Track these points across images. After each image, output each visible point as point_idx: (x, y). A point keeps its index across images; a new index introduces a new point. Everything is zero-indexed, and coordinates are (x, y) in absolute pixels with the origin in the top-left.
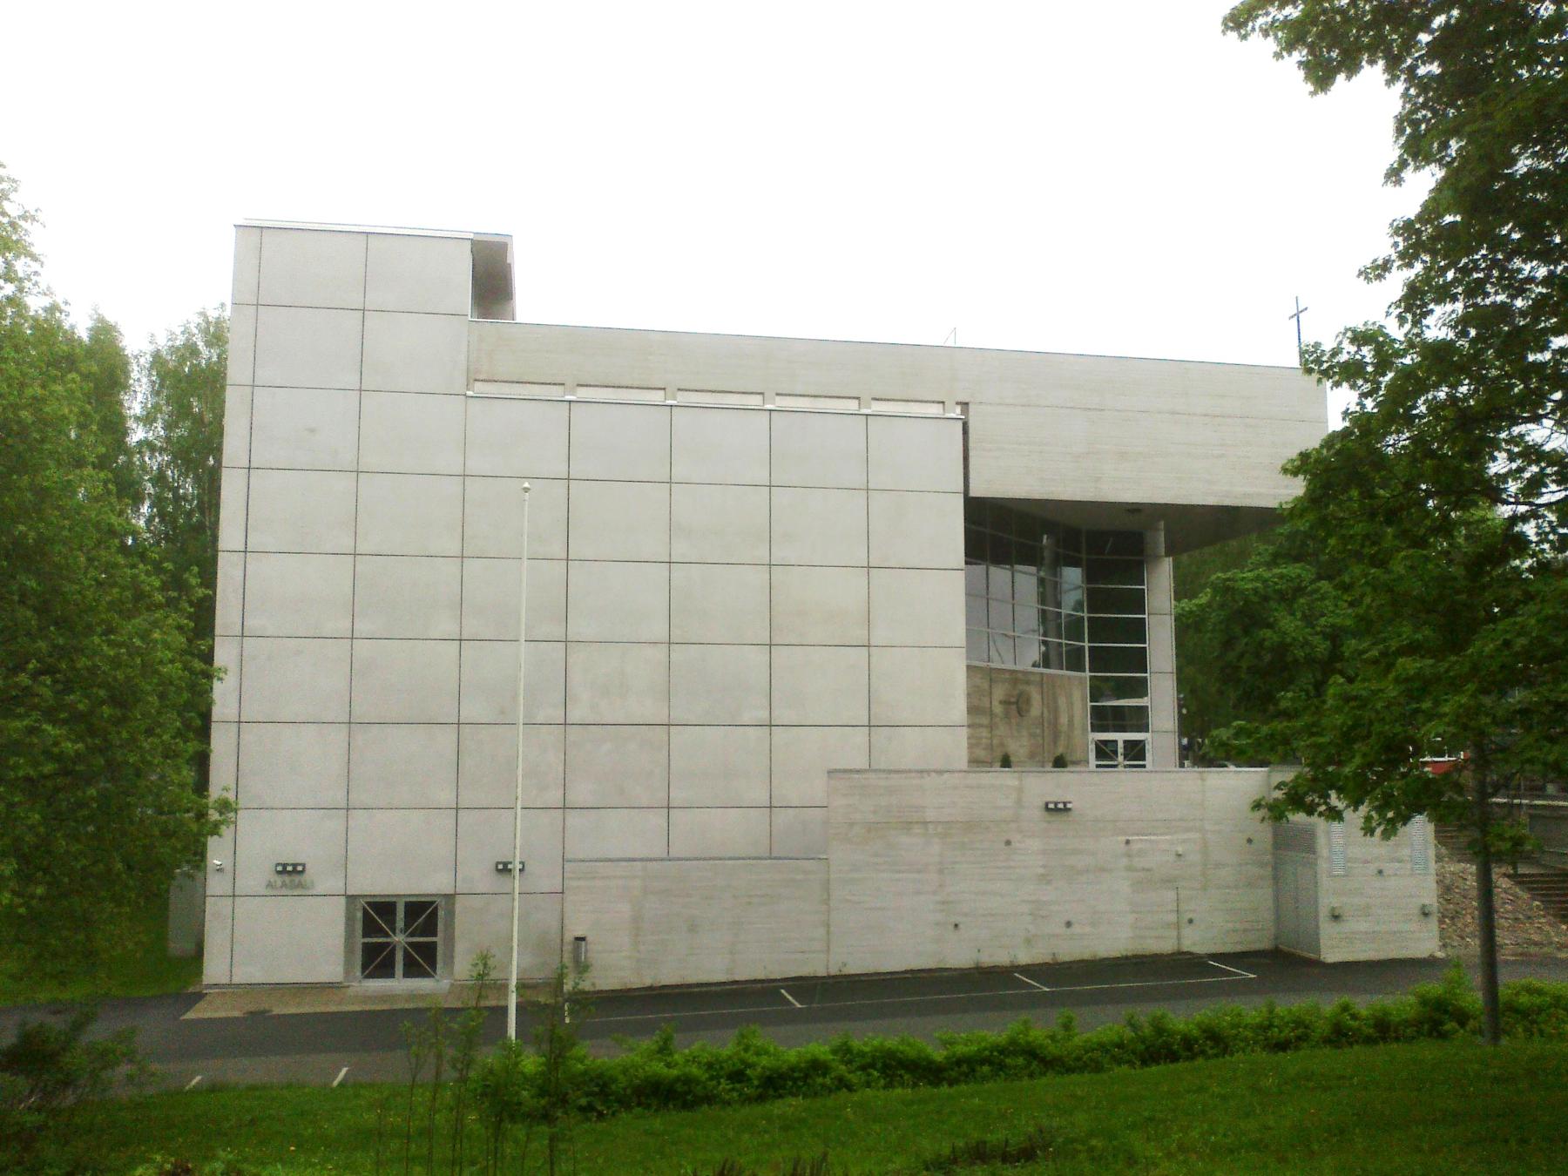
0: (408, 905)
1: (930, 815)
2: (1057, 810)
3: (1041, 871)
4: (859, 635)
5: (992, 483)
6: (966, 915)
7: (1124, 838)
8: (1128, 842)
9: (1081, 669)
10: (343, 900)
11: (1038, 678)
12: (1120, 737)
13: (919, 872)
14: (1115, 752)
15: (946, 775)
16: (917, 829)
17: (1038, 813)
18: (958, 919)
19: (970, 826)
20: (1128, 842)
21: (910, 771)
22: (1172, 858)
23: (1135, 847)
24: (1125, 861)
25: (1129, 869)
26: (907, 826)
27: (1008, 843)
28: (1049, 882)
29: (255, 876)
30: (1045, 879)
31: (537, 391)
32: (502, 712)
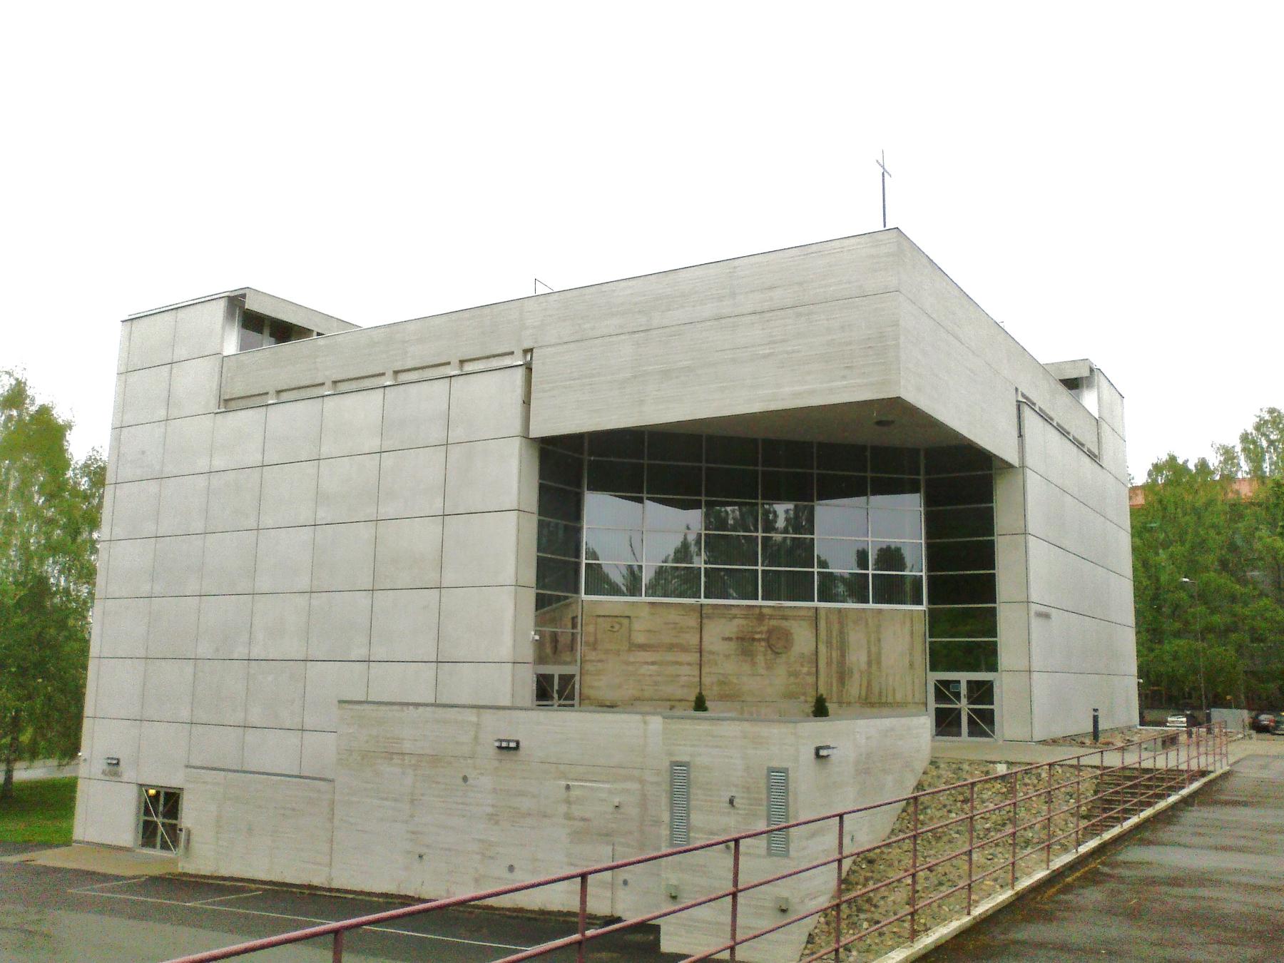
0: (166, 794)
1: (407, 746)
2: (509, 748)
3: (490, 810)
4: (431, 577)
5: (550, 424)
6: (428, 846)
7: (564, 783)
8: (568, 787)
9: (920, 603)
10: (135, 789)
11: (811, 613)
12: (964, 677)
13: (396, 800)
14: (957, 696)
15: (421, 709)
16: (396, 760)
17: (491, 751)
18: (423, 850)
19: (436, 760)
20: (568, 787)
21: (464, 706)
22: (611, 809)
23: (574, 793)
24: (563, 808)
25: (568, 817)
26: (390, 755)
27: (465, 779)
28: (497, 823)
29: (98, 766)
30: (493, 818)
31: (304, 393)
32: (217, 650)
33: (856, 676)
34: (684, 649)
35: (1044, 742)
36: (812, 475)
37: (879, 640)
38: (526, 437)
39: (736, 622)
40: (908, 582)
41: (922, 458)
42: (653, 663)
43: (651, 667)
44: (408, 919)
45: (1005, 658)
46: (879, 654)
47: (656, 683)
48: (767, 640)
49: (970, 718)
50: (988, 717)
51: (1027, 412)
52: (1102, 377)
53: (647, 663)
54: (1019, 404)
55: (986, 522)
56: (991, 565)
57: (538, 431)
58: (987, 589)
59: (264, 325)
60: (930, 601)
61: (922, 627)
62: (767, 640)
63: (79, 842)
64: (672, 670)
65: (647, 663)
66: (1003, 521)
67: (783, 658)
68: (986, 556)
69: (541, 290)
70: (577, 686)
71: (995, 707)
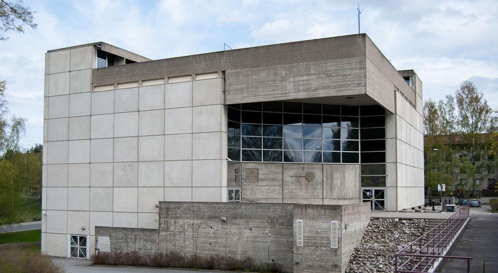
12: (373, 189)
33: (336, 189)
34: (276, 180)
35: (399, 211)
36: (323, 114)
37: (344, 176)
38: (224, 105)
39: (295, 170)
40: (245, 134)
41: (280, 150)
42: (266, 186)
43: (266, 187)
44: (377, 50)
45: (389, 181)
46: (344, 181)
47: (268, 193)
48: (306, 177)
49: (375, 204)
50: (382, 203)
51: (398, 94)
52: (53, 261)
53: (264, 186)
54: (395, 91)
55: (382, 134)
56: (384, 149)
57: (228, 103)
58: (382, 158)
59: (109, 57)
60: (362, 162)
61: (358, 171)
62: (306, 177)
63: (329, 127)
64: (273, 188)
65: (264, 186)
66: (389, 133)
67: (311, 183)
68: (382, 145)
69: (227, 49)
70: (240, 194)
71: (385, 200)
